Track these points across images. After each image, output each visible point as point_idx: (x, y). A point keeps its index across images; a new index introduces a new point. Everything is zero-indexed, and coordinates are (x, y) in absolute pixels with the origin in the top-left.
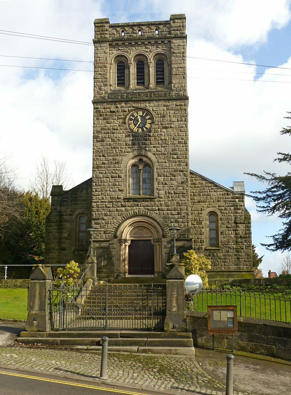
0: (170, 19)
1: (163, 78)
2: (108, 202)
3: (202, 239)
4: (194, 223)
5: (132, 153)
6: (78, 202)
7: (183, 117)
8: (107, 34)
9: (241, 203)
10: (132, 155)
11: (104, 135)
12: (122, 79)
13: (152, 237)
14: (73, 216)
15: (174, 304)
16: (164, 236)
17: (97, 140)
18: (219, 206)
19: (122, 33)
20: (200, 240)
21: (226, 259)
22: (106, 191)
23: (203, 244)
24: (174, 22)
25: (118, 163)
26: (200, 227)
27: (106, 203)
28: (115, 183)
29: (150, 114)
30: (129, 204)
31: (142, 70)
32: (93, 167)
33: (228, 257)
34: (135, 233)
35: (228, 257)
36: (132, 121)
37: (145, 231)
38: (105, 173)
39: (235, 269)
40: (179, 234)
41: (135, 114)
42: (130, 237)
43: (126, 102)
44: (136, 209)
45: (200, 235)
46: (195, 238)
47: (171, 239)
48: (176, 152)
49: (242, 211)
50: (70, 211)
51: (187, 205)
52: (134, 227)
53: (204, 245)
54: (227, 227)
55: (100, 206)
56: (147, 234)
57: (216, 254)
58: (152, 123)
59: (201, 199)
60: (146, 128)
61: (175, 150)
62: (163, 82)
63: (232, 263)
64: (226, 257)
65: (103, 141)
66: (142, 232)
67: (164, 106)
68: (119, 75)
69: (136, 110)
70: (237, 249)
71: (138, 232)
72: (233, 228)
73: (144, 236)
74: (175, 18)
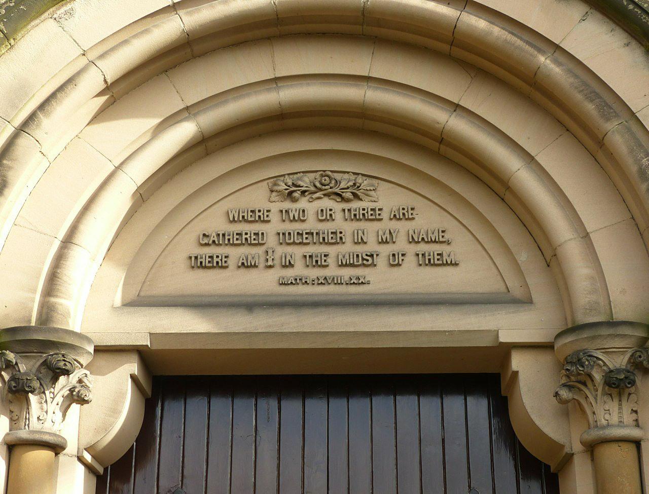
13: (526, 301)
19: (41, 420)
34: (222, 239)
42: (138, 302)
52: (212, 118)
56: (427, 261)
66: (339, 223)
71: (275, 225)
73: (381, 280)
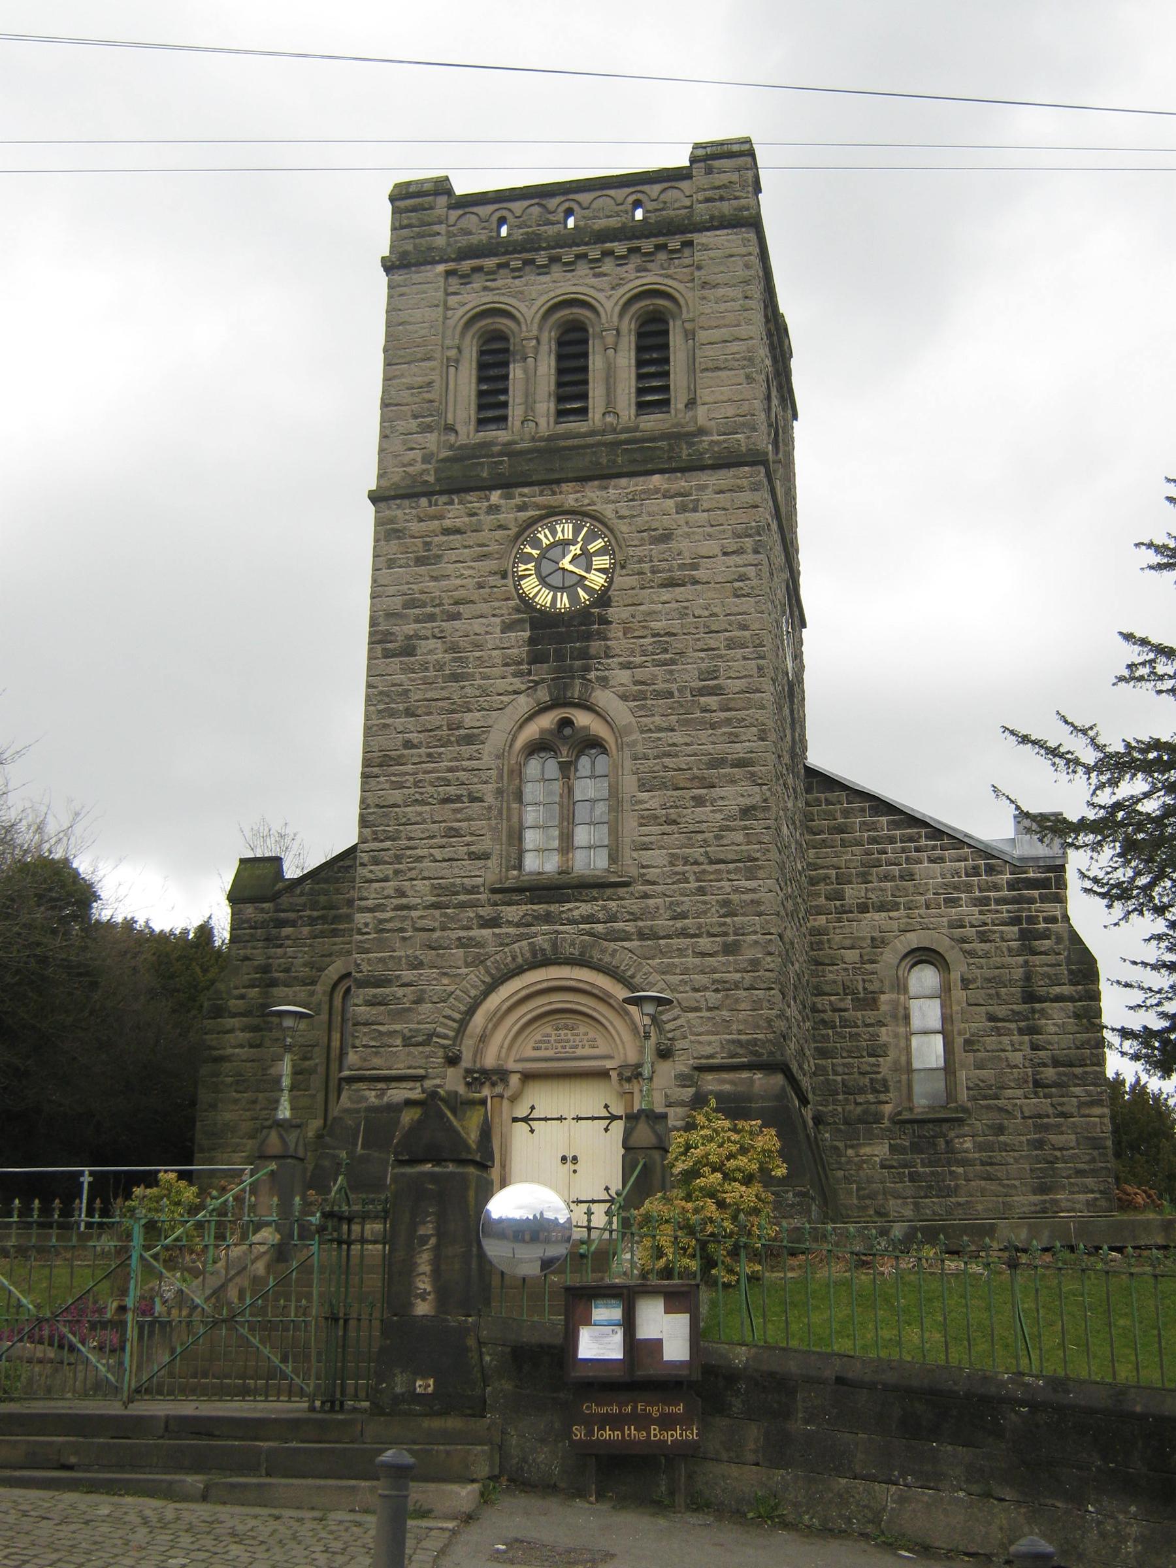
0: (692, 162)
1: (666, 389)
2: (426, 908)
3: (879, 1076)
4: (842, 1005)
5: (528, 696)
6: (341, 927)
7: (747, 536)
8: (439, 234)
9: (1053, 909)
10: (527, 703)
11: (410, 628)
12: (492, 403)
14: (319, 988)
15: (424, 1284)
16: (664, 1054)
17: (384, 649)
18: (951, 926)
20: (871, 1080)
21: (991, 1164)
22: (419, 859)
23: (883, 1097)
24: (709, 171)
25: (469, 740)
26: (869, 1021)
27: (414, 914)
28: (456, 825)
29: (607, 533)
30: (512, 913)
31: (587, 363)
32: (367, 763)
33: (998, 1156)
34: (540, 1042)
35: (998, 1156)
36: (529, 566)
37: (586, 1034)
38: (416, 784)
39: (1033, 1208)
40: (728, 1041)
41: (541, 536)
43: (507, 485)
44: (542, 935)
45: (870, 1055)
46: (846, 1071)
47: (691, 1062)
48: (715, 682)
49: (1057, 943)
50: (305, 965)
51: (762, 908)
53: (887, 1103)
54: (992, 1018)
55: (388, 926)
57: (947, 1142)
58: (614, 569)
59: (870, 895)
60: (587, 589)
61: (712, 674)
62: (666, 403)
63: (1017, 1183)
64: (990, 1157)
65: (409, 651)
66: (569, 1037)
67: (665, 497)
68: (485, 387)
69: (546, 521)
70: (1040, 1116)
72: (1016, 1021)
73: (580, 1052)
74: (709, 156)
